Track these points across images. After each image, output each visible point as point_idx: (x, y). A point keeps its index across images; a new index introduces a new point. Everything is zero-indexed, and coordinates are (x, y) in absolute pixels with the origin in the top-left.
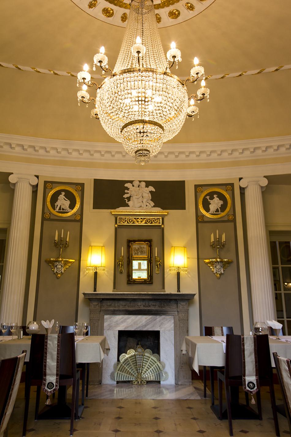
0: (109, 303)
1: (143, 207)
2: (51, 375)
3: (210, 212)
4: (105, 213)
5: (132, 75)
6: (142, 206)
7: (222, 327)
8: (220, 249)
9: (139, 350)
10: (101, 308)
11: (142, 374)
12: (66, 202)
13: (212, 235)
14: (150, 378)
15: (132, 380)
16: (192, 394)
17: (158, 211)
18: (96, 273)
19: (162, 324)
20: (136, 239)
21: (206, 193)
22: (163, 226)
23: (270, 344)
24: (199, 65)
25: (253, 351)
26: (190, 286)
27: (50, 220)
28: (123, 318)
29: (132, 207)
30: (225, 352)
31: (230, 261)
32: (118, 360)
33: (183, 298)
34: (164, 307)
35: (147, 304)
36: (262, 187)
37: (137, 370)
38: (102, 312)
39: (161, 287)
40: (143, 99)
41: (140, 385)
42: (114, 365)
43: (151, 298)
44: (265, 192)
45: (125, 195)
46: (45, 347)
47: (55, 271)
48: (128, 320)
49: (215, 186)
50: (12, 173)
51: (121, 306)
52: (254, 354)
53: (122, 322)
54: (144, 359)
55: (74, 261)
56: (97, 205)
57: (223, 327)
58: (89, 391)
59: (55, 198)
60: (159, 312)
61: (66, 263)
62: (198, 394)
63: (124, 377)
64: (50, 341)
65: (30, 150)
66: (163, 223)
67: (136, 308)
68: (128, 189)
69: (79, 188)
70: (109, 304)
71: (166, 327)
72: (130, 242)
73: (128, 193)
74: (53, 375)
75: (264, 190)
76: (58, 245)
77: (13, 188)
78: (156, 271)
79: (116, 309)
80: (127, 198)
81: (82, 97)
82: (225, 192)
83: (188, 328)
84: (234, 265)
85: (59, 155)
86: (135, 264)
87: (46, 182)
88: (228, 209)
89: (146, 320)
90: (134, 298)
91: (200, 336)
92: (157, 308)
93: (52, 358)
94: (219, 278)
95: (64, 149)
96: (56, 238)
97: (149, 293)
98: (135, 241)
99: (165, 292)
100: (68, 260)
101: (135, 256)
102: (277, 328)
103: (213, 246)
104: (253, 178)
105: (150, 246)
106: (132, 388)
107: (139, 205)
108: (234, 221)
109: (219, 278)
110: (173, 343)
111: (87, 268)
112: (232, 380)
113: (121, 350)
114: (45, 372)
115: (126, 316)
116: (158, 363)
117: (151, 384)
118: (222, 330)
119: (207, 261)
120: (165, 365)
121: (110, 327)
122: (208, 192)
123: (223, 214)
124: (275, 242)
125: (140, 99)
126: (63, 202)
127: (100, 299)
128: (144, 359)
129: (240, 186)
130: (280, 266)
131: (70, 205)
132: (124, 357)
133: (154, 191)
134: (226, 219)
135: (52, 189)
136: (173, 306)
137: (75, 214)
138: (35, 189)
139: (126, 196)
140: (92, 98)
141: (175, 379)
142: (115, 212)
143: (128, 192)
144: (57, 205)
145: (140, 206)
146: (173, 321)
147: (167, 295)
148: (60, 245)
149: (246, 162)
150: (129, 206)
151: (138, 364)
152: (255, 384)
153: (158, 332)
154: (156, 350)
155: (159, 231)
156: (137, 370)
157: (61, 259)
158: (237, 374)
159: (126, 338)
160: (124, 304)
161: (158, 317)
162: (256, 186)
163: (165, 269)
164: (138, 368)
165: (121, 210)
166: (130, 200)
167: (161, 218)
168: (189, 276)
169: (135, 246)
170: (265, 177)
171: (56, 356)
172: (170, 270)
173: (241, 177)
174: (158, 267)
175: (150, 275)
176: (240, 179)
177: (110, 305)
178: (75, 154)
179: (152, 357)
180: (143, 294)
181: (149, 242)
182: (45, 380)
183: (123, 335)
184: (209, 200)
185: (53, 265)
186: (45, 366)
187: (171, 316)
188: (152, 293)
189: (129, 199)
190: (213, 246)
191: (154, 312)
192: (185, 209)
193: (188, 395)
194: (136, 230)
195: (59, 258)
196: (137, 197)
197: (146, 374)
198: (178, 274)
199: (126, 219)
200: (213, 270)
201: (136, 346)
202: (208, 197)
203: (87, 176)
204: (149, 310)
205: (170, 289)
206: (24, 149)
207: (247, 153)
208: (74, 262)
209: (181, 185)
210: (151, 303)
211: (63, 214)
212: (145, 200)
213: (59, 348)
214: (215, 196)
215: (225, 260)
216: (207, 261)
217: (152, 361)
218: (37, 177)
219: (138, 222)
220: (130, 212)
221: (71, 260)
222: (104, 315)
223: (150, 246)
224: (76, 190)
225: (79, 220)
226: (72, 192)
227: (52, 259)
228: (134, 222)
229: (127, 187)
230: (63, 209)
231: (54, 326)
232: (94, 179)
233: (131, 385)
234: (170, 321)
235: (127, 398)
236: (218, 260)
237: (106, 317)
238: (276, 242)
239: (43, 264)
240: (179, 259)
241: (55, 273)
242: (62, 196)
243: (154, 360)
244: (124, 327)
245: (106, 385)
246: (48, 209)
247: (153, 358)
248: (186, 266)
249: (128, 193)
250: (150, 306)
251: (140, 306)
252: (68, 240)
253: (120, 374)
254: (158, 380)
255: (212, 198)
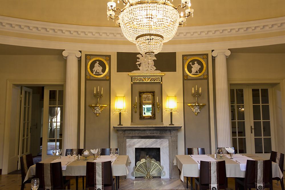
0: (129, 132)
1: (149, 71)
2: (99, 184)
3: (192, 73)
4: (125, 74)
5: (143, 5)
6: (148, 70)
7: (198, 148)
8: (198, 97)
9: (148, 159)
10: (124, 135)
11: (150, 173)
12: (100, 68)
13: (193, 89)
14: (156, 175)
15: (144, 176)
16: (179, 186)
17: (158, 73)
18: (120, 113)
19: (161, 144)
20: (145, 91)
21: (189, 60)
22: (161, 83)
23: (226, 164)
24: (191, 8)
25: (216, 170)
26: (179, 122)
27: (90, 80)
28: (138, 140)
29: (142, 70)
30: (199, 169)
31: (204, 104)
32: (136, 165)
33: (174, 129)
34: (162, 134)
35: (152, 132)
36: (226, 56)
37: (147, 171)
38: (125, 137)
39: (160, 120)
40: (150, 16)
41: (149, 179)
42: (133, 168)
43: (154, 129)
44: (228, 59)
45: (137, 62)
46: (95, 169)
47: (95, 112)
48: (141, 142)
49: (196, 56)
50: (65, 50)
51: (137, 134)
52: (216, 172)
53: (137, 143)
54: (151, 164)
55: (106, 105)
56: (120, 69)
57: (199, 148)
58: (119, 184)
59: (92, 66)
60: (160, 137)
61: (102, 107)
62: (183, 186)
63: (139, 174)
64: (97, 166)
65: (75, 34)
66: (161, 81)
67: (146, 135)
68: (139, 58)
69: (108, 58)
70: (129, 132)
71: (163, 145)
72: (141, 93)
73: (139, 61)
74: (100, 184)
75: (227, 57)
76: (96, 96)
77: (65, 58)
78: (157, 112)
79: (134, 135)
80: (138, 64)
81: (110, 15)
82: (202, 60)
83: (177, 146)
84: (207, 107)
85: (94, 36)
86: (145, 107)
87: (86, 55)
88: (204, 71)
89: (151, 142)
90: (144, 129)
91: (185, 154)
92: (158, 135)
93: (99, 176)
94: (197, 115)
95: (97, 33)
96: (95, 93)
97: (154, 126)
98: (144, 93)
99: (163, 124)
100: (103, 105)
101: (144, 102)
102: (231, 152)
103: (194, 95)
104: (220, 51)
105: (154, 96)
106: (144, 181)
107: (146, 69)
108: (207, 79)
109: (197, 115)
110: (168, 155)
111: (115, 110)
112: (193, 15)
113: (137, 159)
114: (96, 183)
115: (140, 140)
116: (159, 167)
117: (155, 178)
118: (198, 150)
119: (189, 105)
120: (163, 167)
121: (130, 146)
122: (191, 60)
123: (200, 74)
124: (234, 90)
125: (148, 16)
126: (98, 68)
127: (124, 130)
128: (151, 164)
129: (212, 56)
130: (237, 121)
131: (102, 70)
132: (139, 163)
133: (156, 59)
134: (202, 77)
135: (90, 59)
136: (168, 133)
137: (105, 76)
138: (80, 60)
139: (137, 63)
140: (116, 15)
141: (170, 176)
142: (131, 74)
143: (139, 60)
144: (94, 70)
145: (147, 70)
146: (168, 142)
147: (164, 127)
148: (98, 96)
149: (217, 42)
150: (140, 70)
151: (147, 167)
152: (217, 188)
153: (159, 149)
154: (157, 158)
155: (159, 86)
156: (147, 171)
157: (98, 105)
158: (206, 183)
159: (140, 152)
160: (138, 132)
161: (159, 140)
162: (223, 56)
163: (163, 110)
164: (148, 170)
165: (135, 73)
166: (140, 66)
167: (160, 77)
168: (178, 113)
169: (144, 96)
170: (228, 49)
171: (101, 174)
172: (166, 111)
173: (213, 49)
174: (158, 109)
175: (154, 114)
176: (213, 51)
177: (130, 133)
178: (104, 36)
179: (156, 163)
180: (150, 127)
181: (153, 93)
182: (96, 187)
183: (139, 151)
184: (191, 65)
185: (94, 108)
186: (96, 180)
187: (166, 139)
188: (155, 126)
189: (140, 65)
190: (194, 95)
191: (156, 137)
192: (176, 71)
193: (178, 186)
194: (144, 85)
195: (97, 105)
196: (145, 64)
197: (152, 172)
198: (171, 113)
199: (138, 78)
200: (193, 110)
201: (146, 156)
202: (191, 63)
203: (112, 50)
204: (153, 136)
205: (166, 123)
206: (71, 33)
207: (218, 33)
208: (106, 106)
209: (174, 55)
210: (155, 132)
211: (98, 76)
212: (150, 66)
213: (103, 170)
214: (195, 62)
215: (201, 104)
216: (189, 105)
217: (156, 165)
218: (81, 52)
219: (146, 80)
220: (140, 74)
221: (104, 105)
222: (126, 139)
223: (154, 96)
224: (106, 60)
225: (108, 79)
226: (102, 60)
227: (93, 105)
228: (143, 80)
229: (138, 57)
230: (98, 73)
231: (98, 152)
232: (117, 52)
233: (144, 179)
234: (166, 142)
235: (142, 189)
236: (197, 104)
237: (127, 140)
238: (234, 89)
239: (88, 108)
240: (172, 103)
241: (95, 113)
242: (97, 64)
243: (157, 165)
244: (138, 146)
245: (129, 179)
246: (88, 72)
247: (156, 163)
248: (176, 108)
249: (139, 61)
250: (154, 134)
251: (148, 134)
252: (102, 93)
253: (137, 173)
254: (160, 176)
255: (193, 64)
